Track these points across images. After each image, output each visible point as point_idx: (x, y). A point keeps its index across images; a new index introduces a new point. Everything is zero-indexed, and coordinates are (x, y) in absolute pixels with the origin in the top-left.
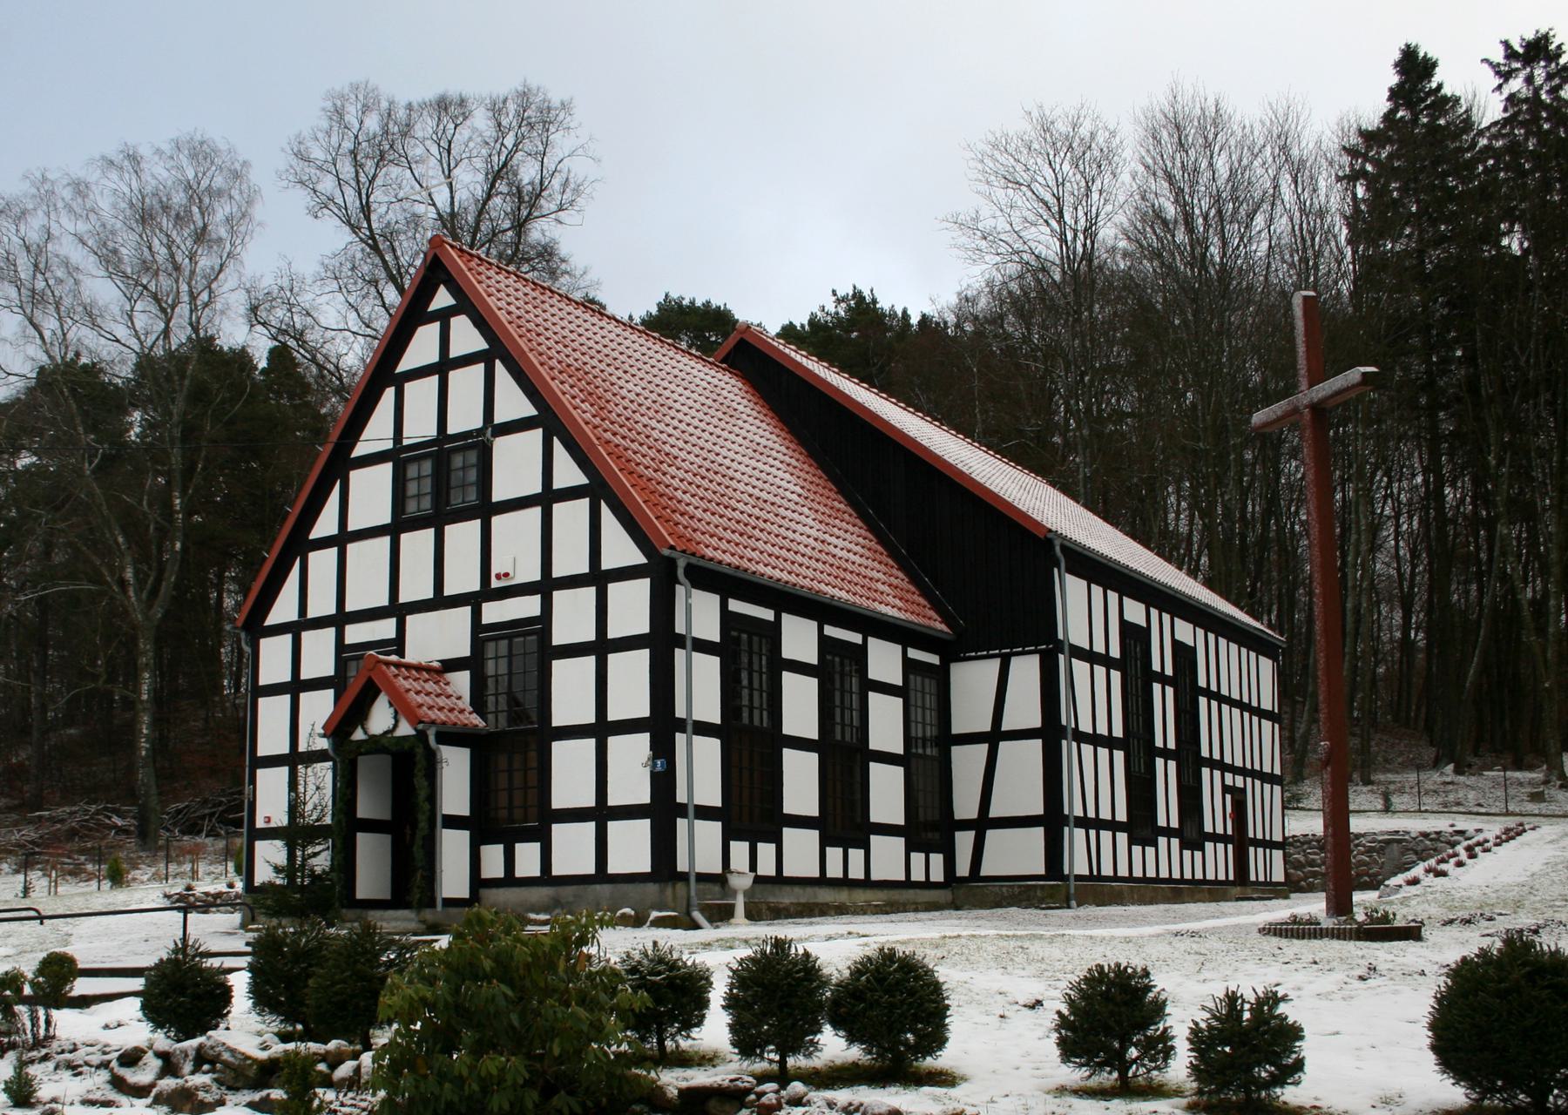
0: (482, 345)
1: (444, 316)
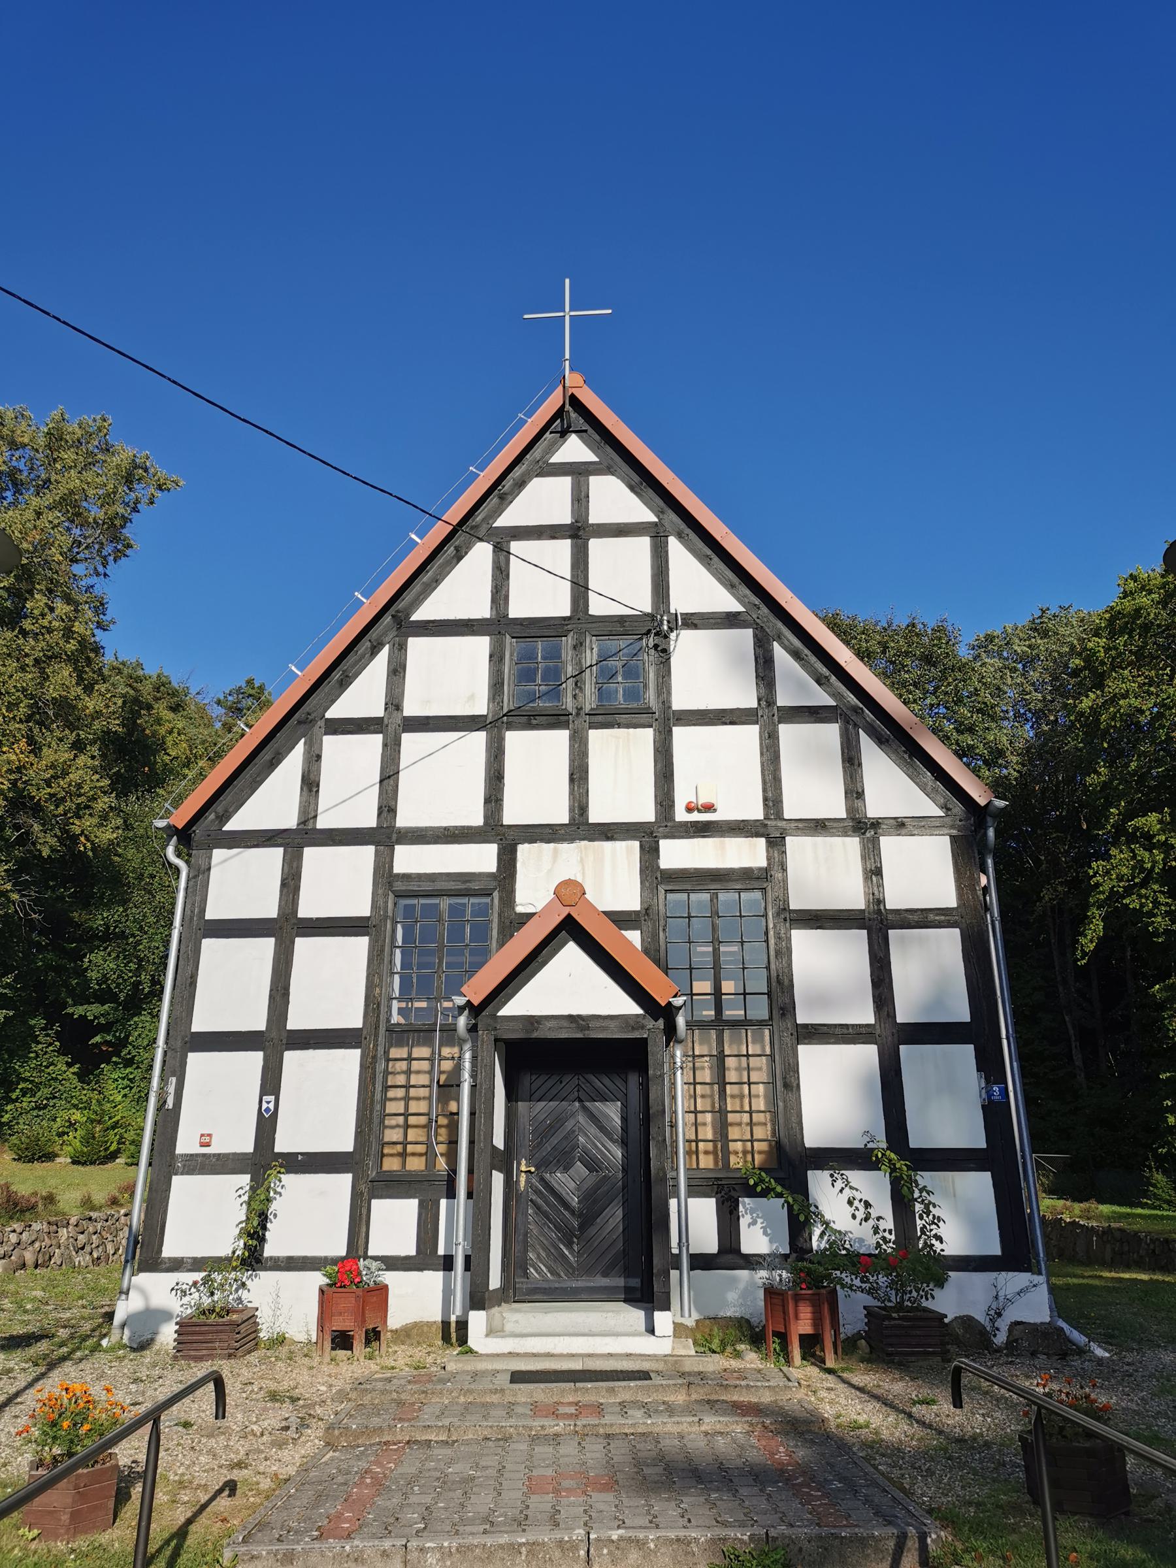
1: (579, 472)
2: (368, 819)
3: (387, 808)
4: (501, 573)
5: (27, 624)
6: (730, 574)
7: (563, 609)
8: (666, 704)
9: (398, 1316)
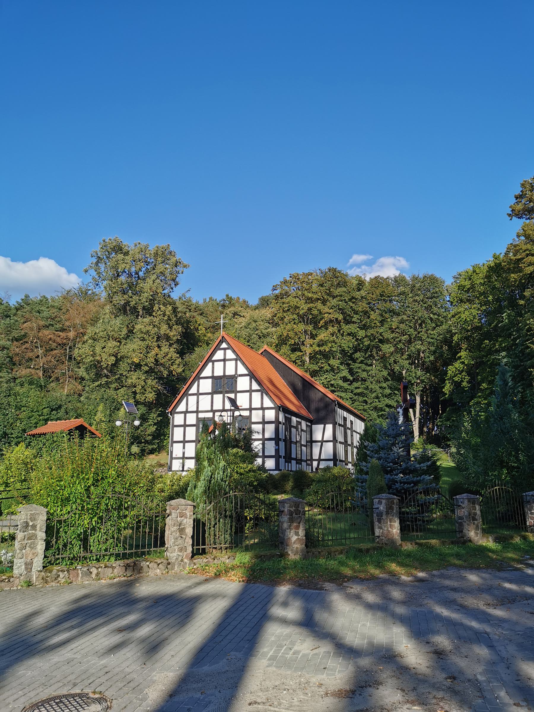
0: (235, 357)
1: (225, 349)
2: (195, 409)
3: (198, 408)
4: (213, 368)
7: (222, 374)
8: (236, 390)
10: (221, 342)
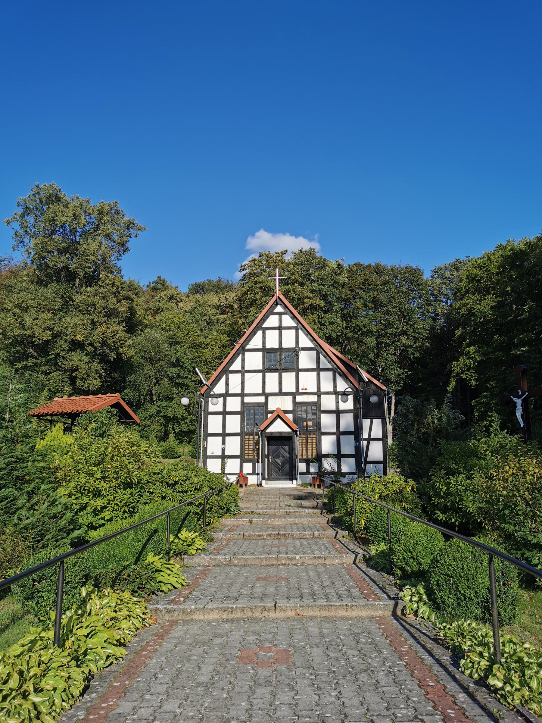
1: (280, 314)
3: (243, 389)
4: (264, 337)
5: (100, 283)
6: (312, 338)
8: (298, 368)
9: (250, 483)
10: (276, 304)
